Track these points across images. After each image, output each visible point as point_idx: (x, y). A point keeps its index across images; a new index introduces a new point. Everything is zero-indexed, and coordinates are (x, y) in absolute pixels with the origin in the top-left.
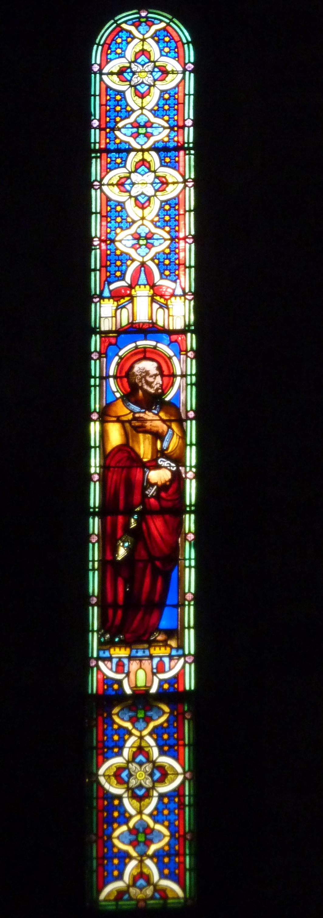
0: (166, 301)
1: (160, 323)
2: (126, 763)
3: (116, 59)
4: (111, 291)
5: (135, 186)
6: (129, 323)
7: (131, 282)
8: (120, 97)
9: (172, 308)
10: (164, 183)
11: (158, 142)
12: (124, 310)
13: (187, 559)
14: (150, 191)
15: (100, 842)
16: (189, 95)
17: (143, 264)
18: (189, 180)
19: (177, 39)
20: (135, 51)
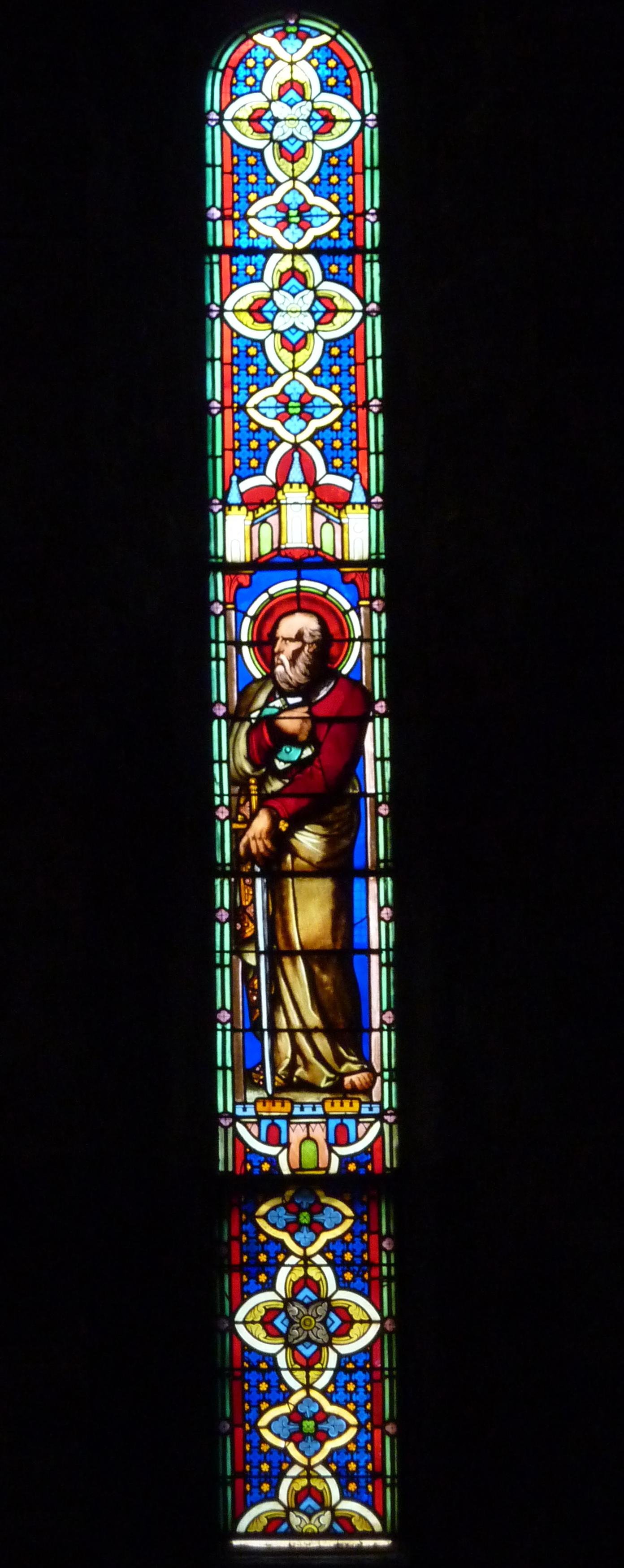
0: (337, 511)
1: (328, 549)
2: (284, 1511)
3: (246, 283)
4: (242, 494)
5: (279, 124)
6: (273, 550)
7: (277, 480)
8: (255, 160)
9: (348, 523)
10: (329, 120)
11: (320, 238)
12: (265, 527)
13: (376, 640)
14: (307, 323)
15: (239, 1432)
16: (374, 358)
17: (296, 447)
18: (389, 1112)
19: (349, 64)
20: (278, 83)
